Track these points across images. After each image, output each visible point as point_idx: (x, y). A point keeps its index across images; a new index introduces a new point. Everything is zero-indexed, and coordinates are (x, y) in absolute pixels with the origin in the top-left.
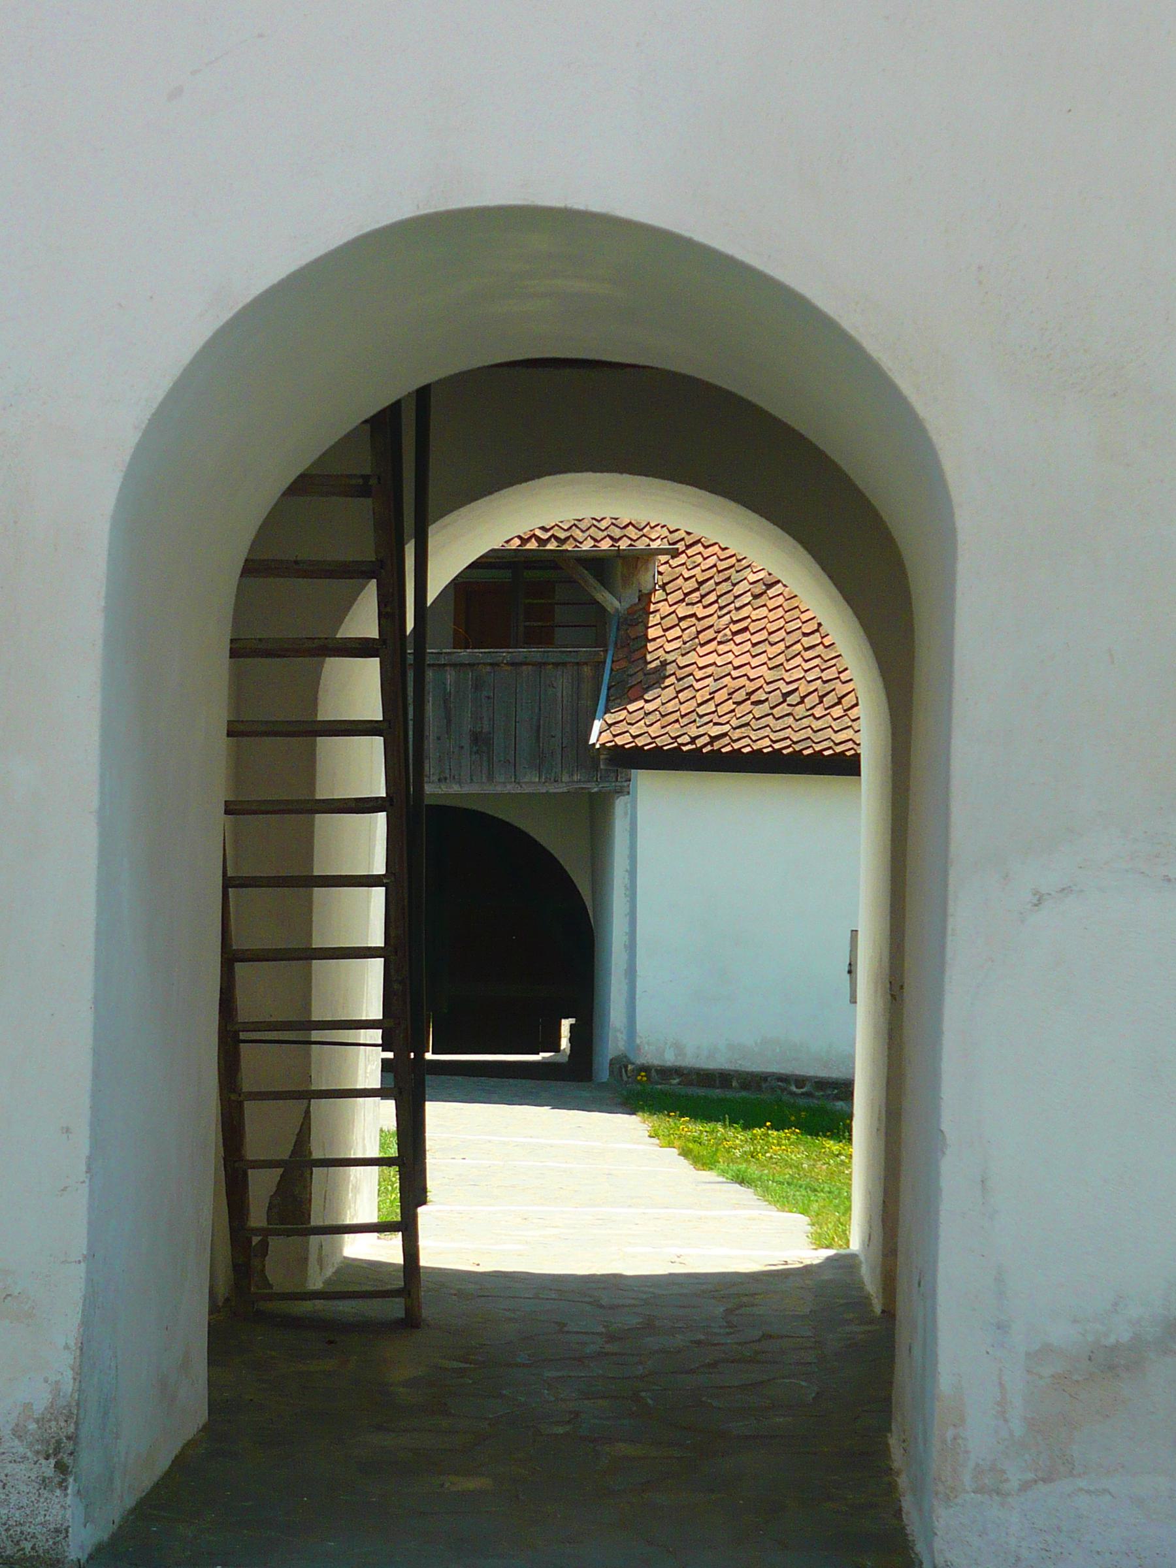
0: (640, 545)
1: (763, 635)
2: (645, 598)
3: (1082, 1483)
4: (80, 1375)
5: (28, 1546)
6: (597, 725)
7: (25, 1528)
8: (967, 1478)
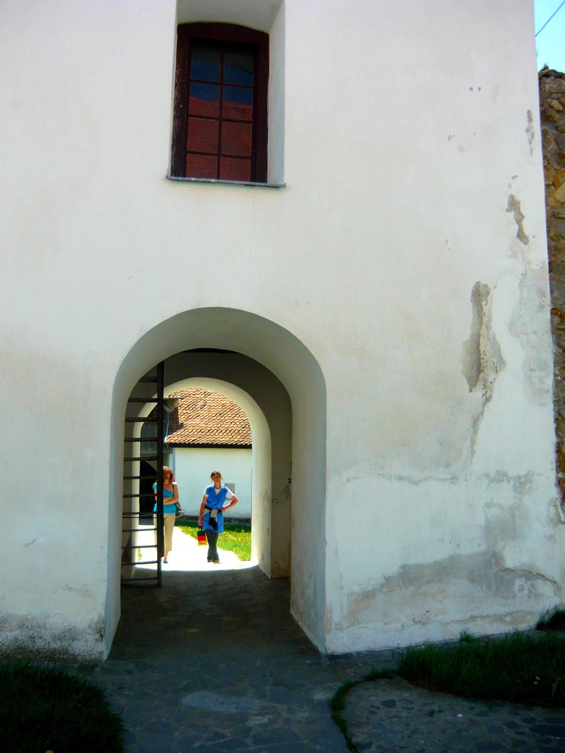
0: (175, 397)
1: (203, 417)
2: (176, 410)
3: (361, 626)
4: (106, 612)
5: (93, 657)
6: (166, 438)
7: (92, 652)
8: (333, 627)
